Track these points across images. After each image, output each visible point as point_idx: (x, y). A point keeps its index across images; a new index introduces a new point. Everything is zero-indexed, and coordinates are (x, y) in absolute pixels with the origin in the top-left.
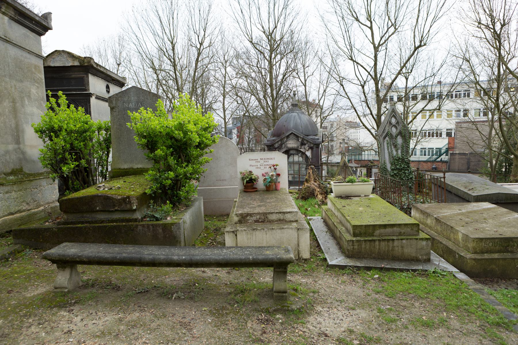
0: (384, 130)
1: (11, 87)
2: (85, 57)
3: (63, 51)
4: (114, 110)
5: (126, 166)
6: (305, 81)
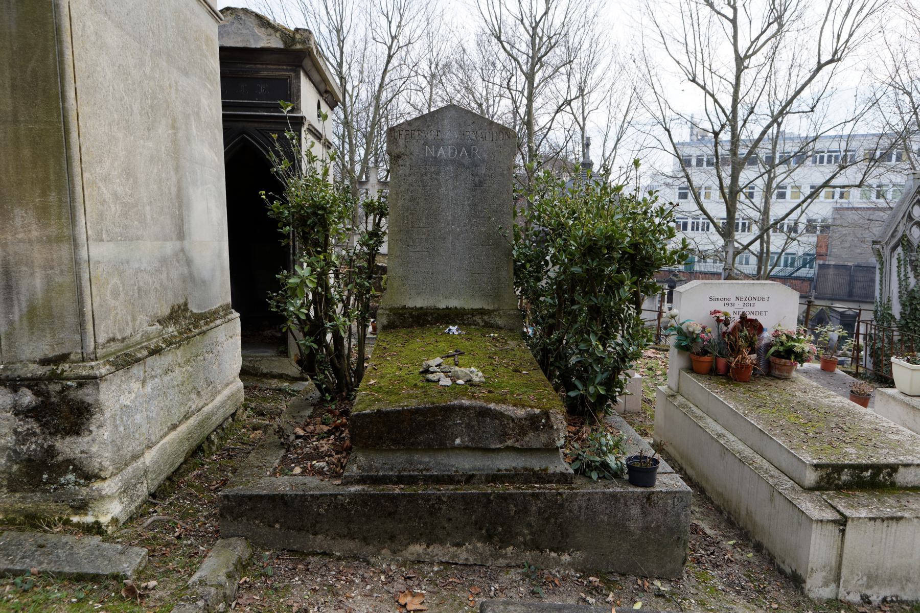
0: (895, 231)
1: (170, 86)
2: (297, 30)
3: (245, 11)
4: (401, 162)
5: (419, 302)
6: (584, 119)
